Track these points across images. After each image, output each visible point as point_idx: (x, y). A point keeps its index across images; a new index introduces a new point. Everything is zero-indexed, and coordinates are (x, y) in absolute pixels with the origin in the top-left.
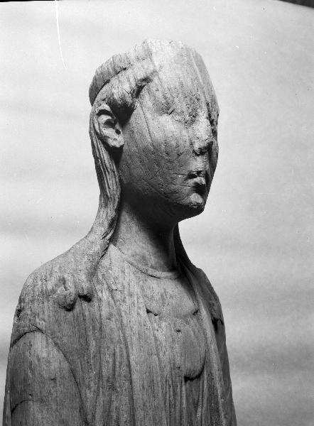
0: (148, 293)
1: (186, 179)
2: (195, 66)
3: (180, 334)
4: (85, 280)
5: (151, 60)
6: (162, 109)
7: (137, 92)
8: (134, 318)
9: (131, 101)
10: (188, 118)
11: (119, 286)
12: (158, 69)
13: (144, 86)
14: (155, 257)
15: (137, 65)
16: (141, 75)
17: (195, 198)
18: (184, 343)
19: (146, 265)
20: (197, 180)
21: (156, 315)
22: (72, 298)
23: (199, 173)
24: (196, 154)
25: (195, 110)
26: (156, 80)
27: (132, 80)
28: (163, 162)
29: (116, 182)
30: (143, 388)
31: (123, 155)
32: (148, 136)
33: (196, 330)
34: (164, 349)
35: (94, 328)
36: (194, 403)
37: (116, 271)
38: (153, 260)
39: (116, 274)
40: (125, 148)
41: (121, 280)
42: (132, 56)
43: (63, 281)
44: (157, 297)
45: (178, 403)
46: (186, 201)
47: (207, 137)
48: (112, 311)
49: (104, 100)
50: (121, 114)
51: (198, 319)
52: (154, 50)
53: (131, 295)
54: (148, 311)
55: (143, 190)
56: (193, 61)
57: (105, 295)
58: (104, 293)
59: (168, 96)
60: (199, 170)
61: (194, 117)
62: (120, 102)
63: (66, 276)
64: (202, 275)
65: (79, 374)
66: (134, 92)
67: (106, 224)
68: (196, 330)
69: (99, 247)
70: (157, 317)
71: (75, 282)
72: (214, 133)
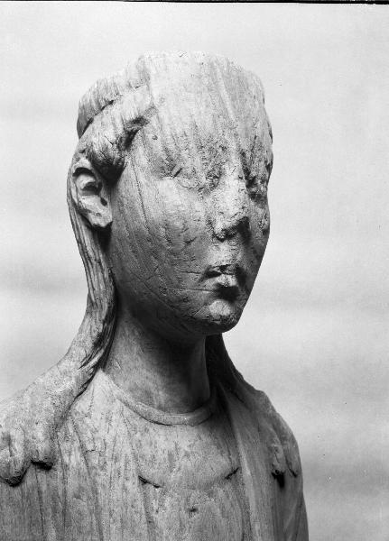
0: (147, 451)
1: (202, 280)
2: (224, 93)
3: (195, 516)
4: (42, 438)
5: (148, 89)
6: (163, 168)
7: (127, 141)
8: (117, 494)
9: (117, 156)
10: (205, 181)
11: (99, 445)
12: (156, 103)
13: (137, 131)
14: (166, 392)
15: (128, 96)
16: (131, 115)
17: (219, 308)
19: (151, 404)
20: (221, 280)
21: (157, 487)
22: (19, 467)
23: (223, 268)
24: (218, 238)
25: (219, 166)
26: (153, 121)
27: (118, 121)
29: (104, 279)
31: (112, 239)
32: (140, 213)
33: (228, 506)
35: (55, 510)
37: (96, 420)
38: (161, 396)
39: (97, 424)
40: (114, 227)
41: (102, 433)
42: (122, 82)
44: (162, 456)
47: (237, 210)
48: (83, 485)
49: (83, 152)
50: (104, 174)
51: (235, 487)
52: (153, 72)
53: (116, 459)
54: (144, 481)
55: (140, 292)
56: (222, 83)
57: (74, 460)
58: (72, 457)
59: (171, 147)
60: (224, 264)
61: (216, 177)
62: (100, 158)
63: (12, 433)
64: (260, 403)
66: (121, 141)
67: (89, 344)
68: (228, 506)
69: (74, 381)
71: (26, 441)
72: (260, 198)
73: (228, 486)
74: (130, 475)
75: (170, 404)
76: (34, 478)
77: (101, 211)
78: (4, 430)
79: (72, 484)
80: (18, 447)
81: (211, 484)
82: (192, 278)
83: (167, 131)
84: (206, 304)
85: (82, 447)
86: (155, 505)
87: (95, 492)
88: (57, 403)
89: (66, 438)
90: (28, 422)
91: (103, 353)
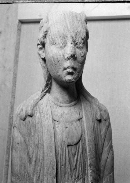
0: (56, 113)
1: (63, 70)
3: (67, 129)
7: (45, 36)
10: (61, 45)
16: (45, 30)
18: (68, 133)
20: (68, 70)
23: (68, 67)
28: (53, 64)
30: (47, 149)
34: (59, 135)
35: (33, 127)
36: (72, 155)
37: (44, 105)
38: (61, 100)
41: (44, 109)
43: (22, 110)
44: (59, 114)
45: (64, 154)
46: (64, 79)
47: (70, 52)
48: (39, 121)
53: (47, 115)
59: (53, 37)
61: (65, 44)
65: (27, 142)
67: (44, 87)
69: (39, 96)
70: (58, 122)
73: (78, 122)
74: (50, 119)
75: (63, 101)
76: (28, 119)
77: (43, 54)
78: (22, 108)
79: (37, 120)
80: (24, 112)
81: (73, 121)
82: (61, 70)
83: (52, 33)
84: (65, 77)
85: (40, 112)
86: (57, 126)
87: (42, 122)
88: (35, 101)
89: (36, 110)
90: (27, 106)
91: (48, 89)
